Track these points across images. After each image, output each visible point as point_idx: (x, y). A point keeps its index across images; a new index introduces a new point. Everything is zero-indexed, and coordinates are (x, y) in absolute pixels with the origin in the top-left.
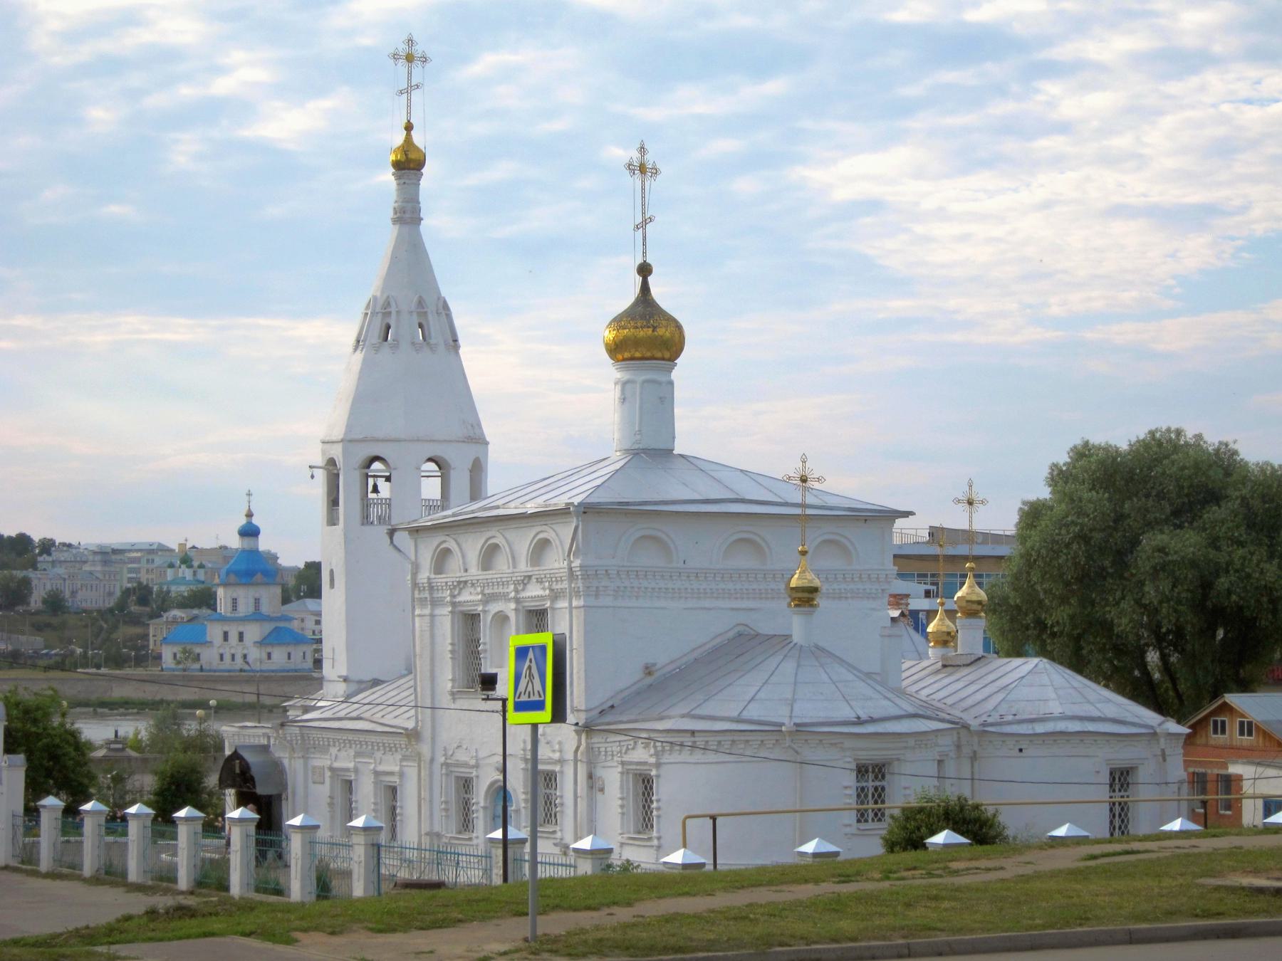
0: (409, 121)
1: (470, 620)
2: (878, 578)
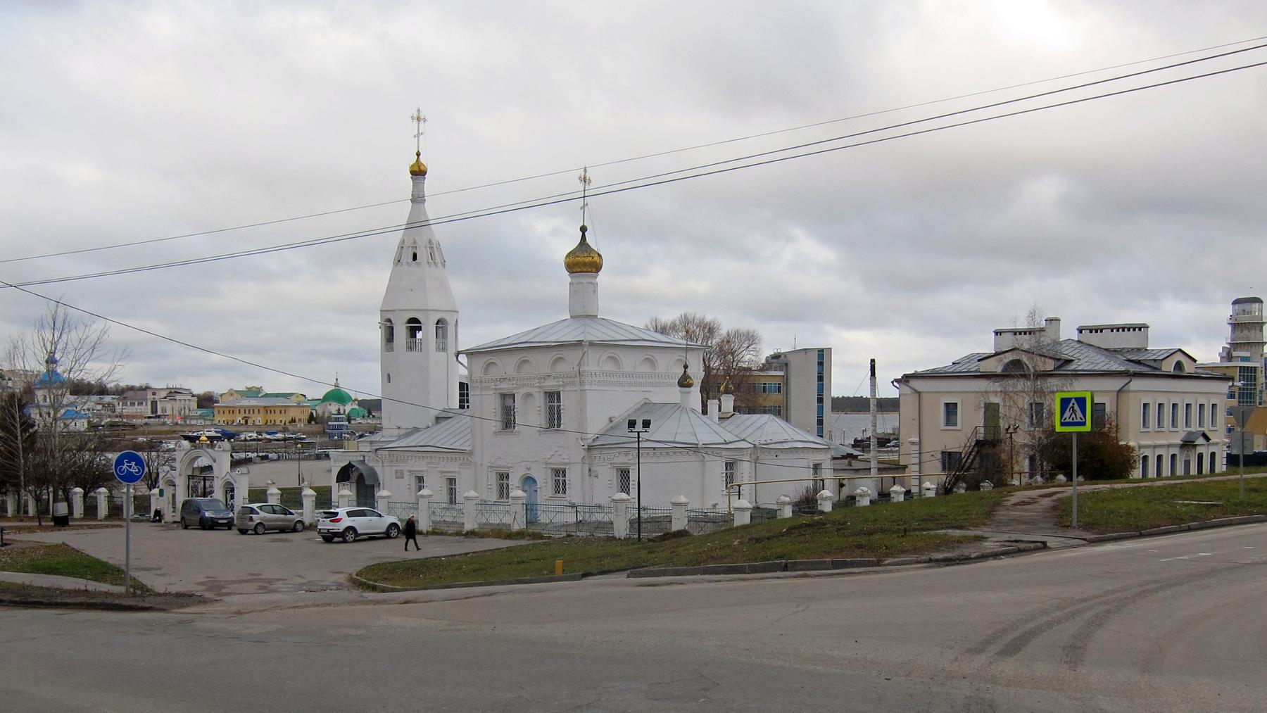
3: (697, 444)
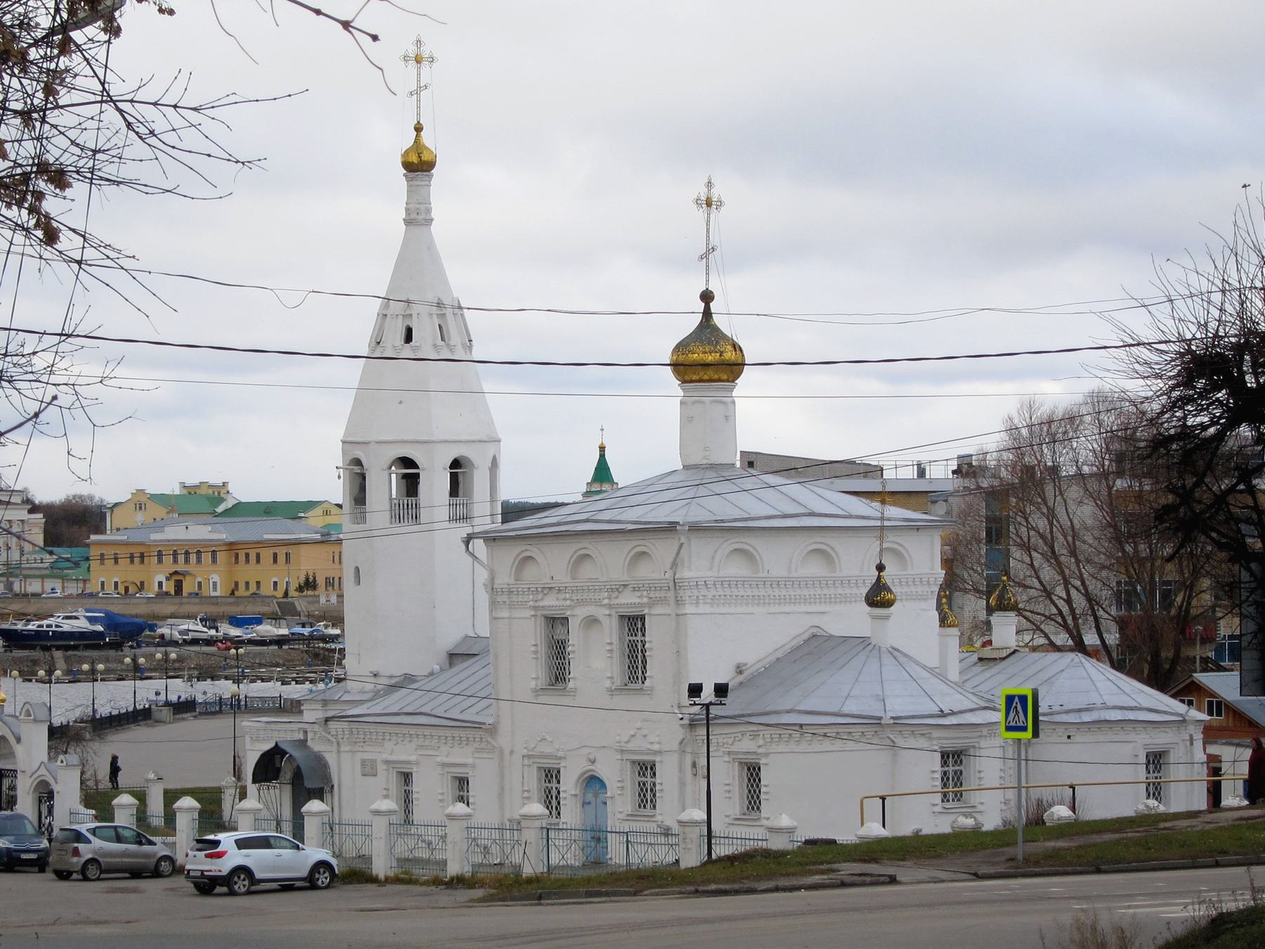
0: (419, 122)
1: (556, 622)
2: (928, 582)
3: (880, 718)
